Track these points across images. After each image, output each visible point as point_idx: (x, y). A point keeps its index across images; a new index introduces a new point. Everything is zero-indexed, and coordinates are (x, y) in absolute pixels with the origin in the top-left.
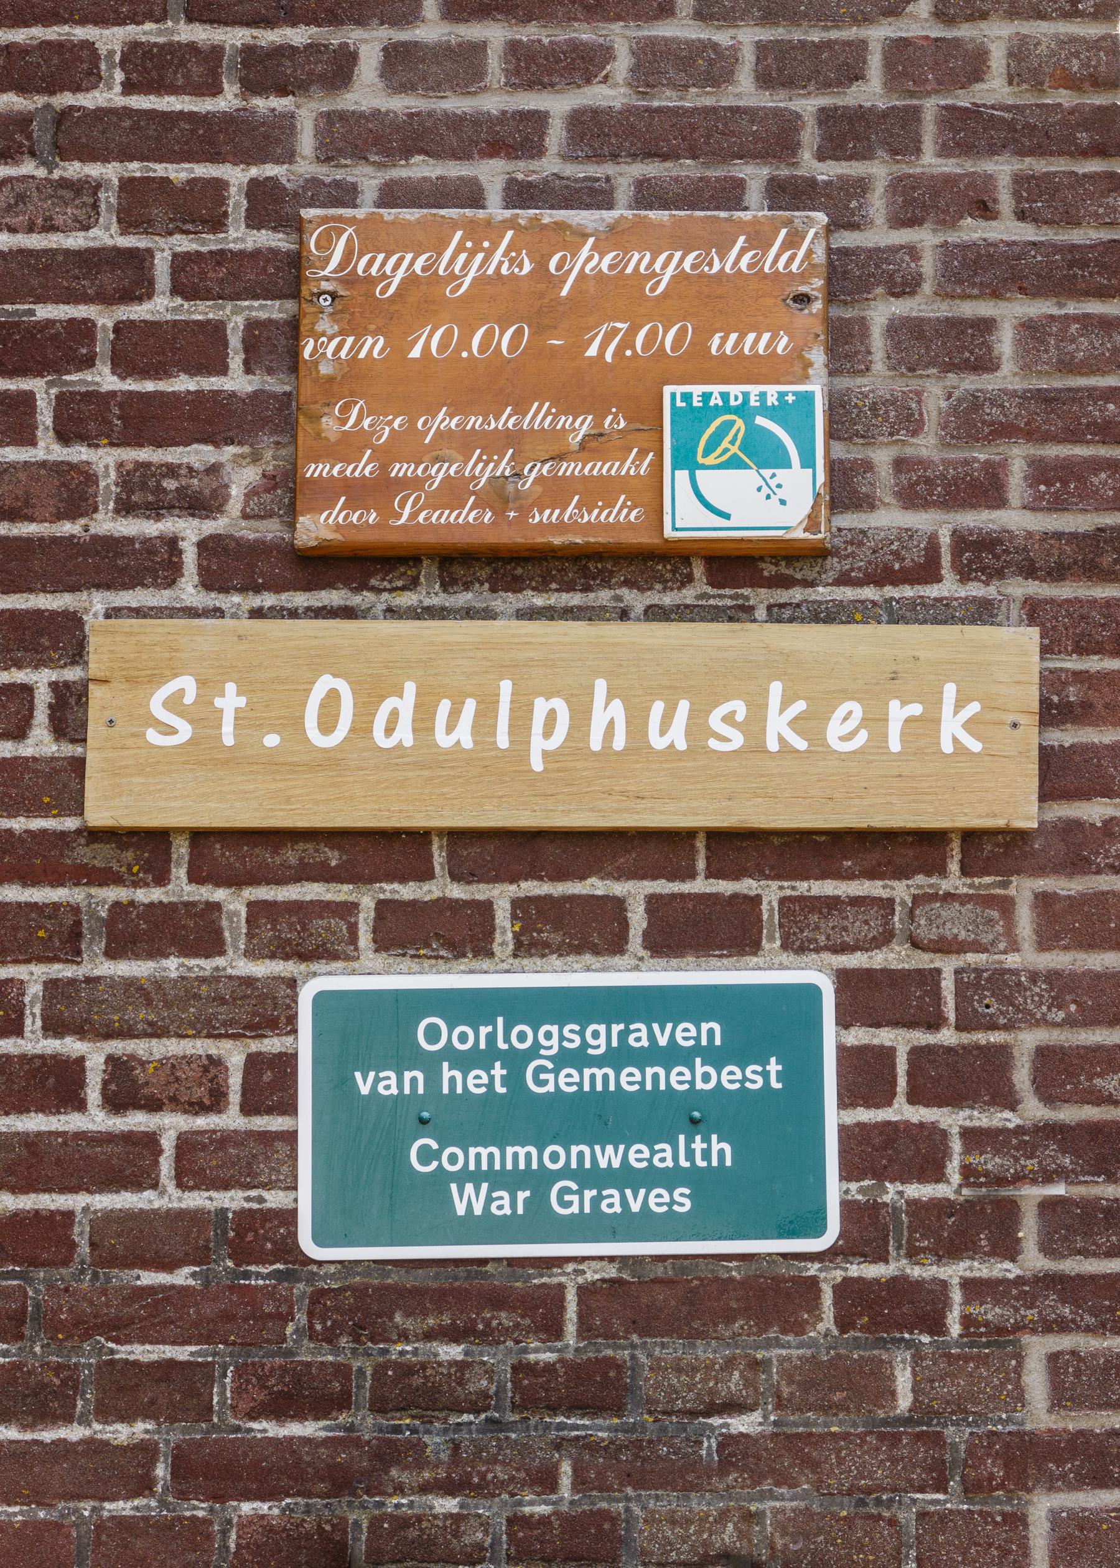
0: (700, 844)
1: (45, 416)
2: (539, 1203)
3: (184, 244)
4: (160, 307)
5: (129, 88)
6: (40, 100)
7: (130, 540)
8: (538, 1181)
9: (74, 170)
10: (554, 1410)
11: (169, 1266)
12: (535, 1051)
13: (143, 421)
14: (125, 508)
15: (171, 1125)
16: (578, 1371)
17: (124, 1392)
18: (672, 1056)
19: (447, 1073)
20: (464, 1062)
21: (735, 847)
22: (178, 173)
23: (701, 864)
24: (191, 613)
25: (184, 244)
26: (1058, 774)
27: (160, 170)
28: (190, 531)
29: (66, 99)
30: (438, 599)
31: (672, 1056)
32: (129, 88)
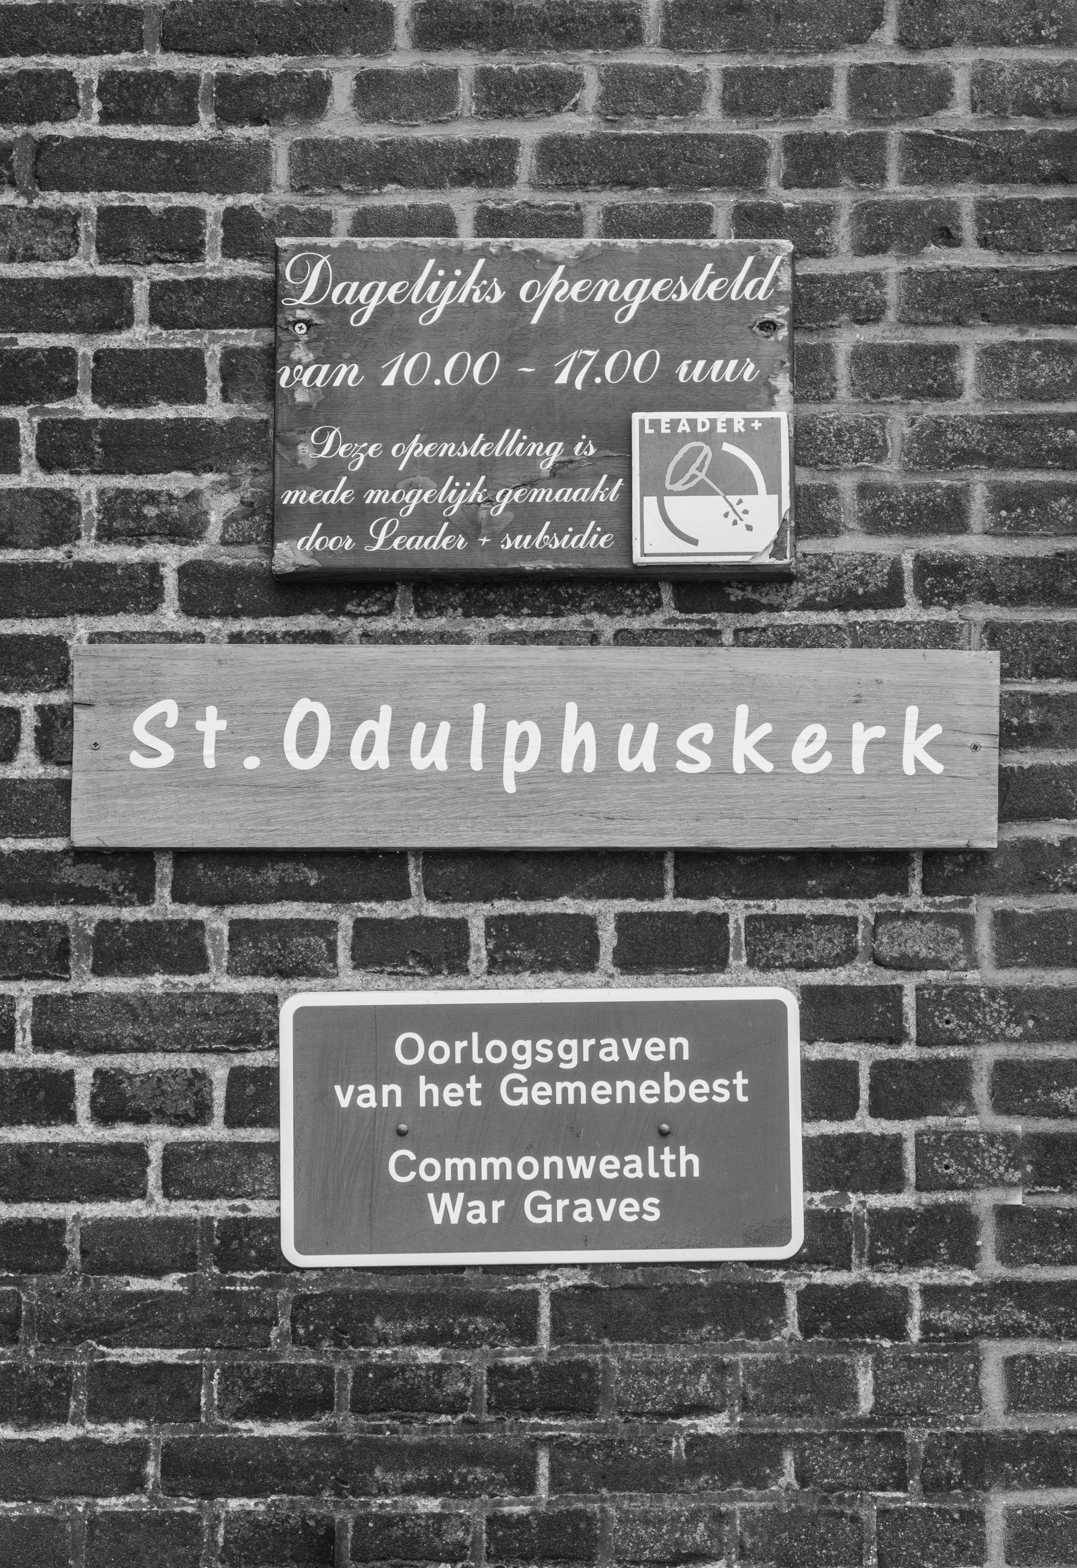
0: (669, 864)
1: (28, 445)
2: (513, 1212)
3: (162, 273)
4: (139, 335)
5: (106, 118)
6: (20, 130)
7: (112, 566)
8: (513, 1191)
9: (53, 199)
10: (528, 1411)
11: (158, 1273)
12: (508, 1065)
13: (125, 449)
14: (107, 535)
15: (158, 1137)
16: (552, 1374)
17: (115, 1393)
18: (642, 1070)
19: (424, 1086)
20: (441, 1075)
21: (703, 867)
22: (155, 202)
23: (670, 884)
24: (172, 637)
25: (162, 273)
26: (1018, 797)
27: (138, 199)
28: (171, 557)
29: (45, 129)
30: (413, 624)
31: (642, 1070)
32: (106, 118)
